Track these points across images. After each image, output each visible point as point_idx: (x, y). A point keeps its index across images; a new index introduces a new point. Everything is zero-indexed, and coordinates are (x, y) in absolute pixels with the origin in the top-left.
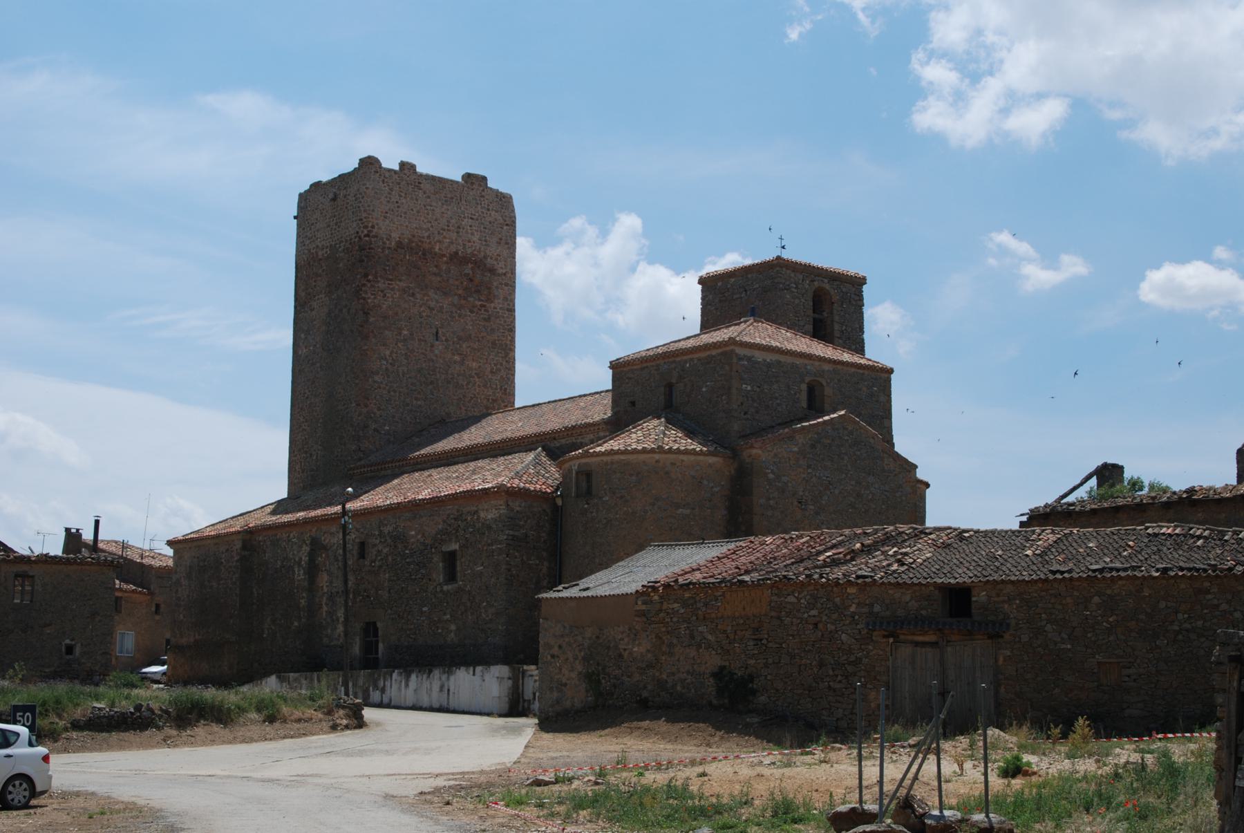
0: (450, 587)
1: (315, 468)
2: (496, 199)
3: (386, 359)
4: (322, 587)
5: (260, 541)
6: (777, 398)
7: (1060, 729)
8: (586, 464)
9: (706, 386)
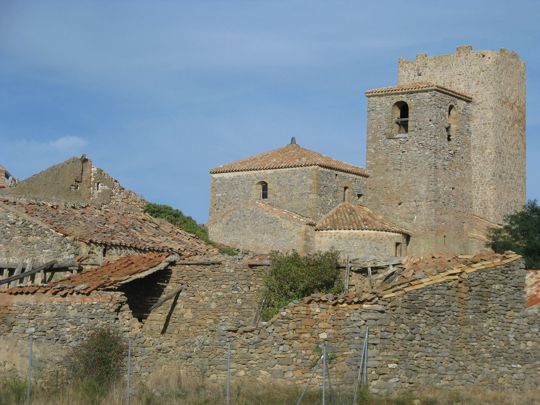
6: (237, 197)
7: (377, 383)
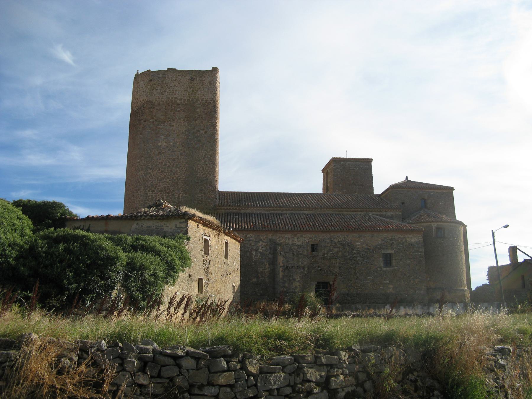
0: (388, 269)
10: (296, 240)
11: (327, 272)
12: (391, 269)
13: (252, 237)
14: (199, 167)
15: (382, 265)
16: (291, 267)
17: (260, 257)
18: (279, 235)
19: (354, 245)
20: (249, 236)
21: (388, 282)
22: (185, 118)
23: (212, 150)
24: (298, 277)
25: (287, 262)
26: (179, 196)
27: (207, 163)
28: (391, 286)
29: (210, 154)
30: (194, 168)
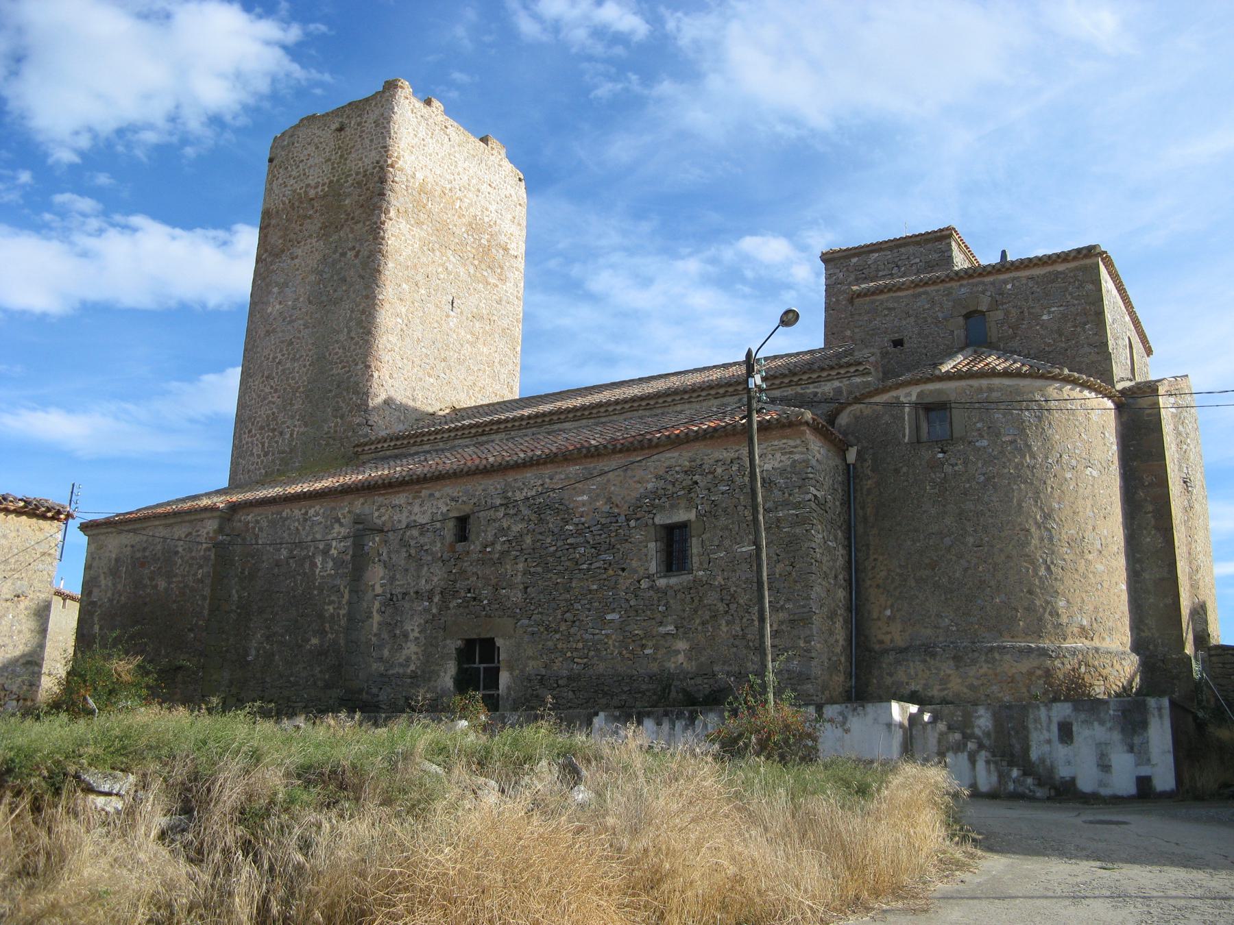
0: (673, 581)
1: (288, 450)
2: (511, 174)
3: (401, 317)
4: (373, 586)
5: (248, 522)
8: (940, 392)
9: (1049, 313)
10: (416, 509)
11: (490, 604)
12: (685, 578)
13: (317, 514)
14: (337, 350)
15: (653, 568)
16: (400, 597)
17: (333, 572)
18: (379, 499)
19: (571, 506)
20: (312, 512)
21: (671, 628)
22: (321, 229)
23: (367, 297)
24: (413, 626)
25: (392, 579)
26: (292, 435)
27: (353, 334)
28: (682, 645)
29: (361, 307)
30: (327, 354)
